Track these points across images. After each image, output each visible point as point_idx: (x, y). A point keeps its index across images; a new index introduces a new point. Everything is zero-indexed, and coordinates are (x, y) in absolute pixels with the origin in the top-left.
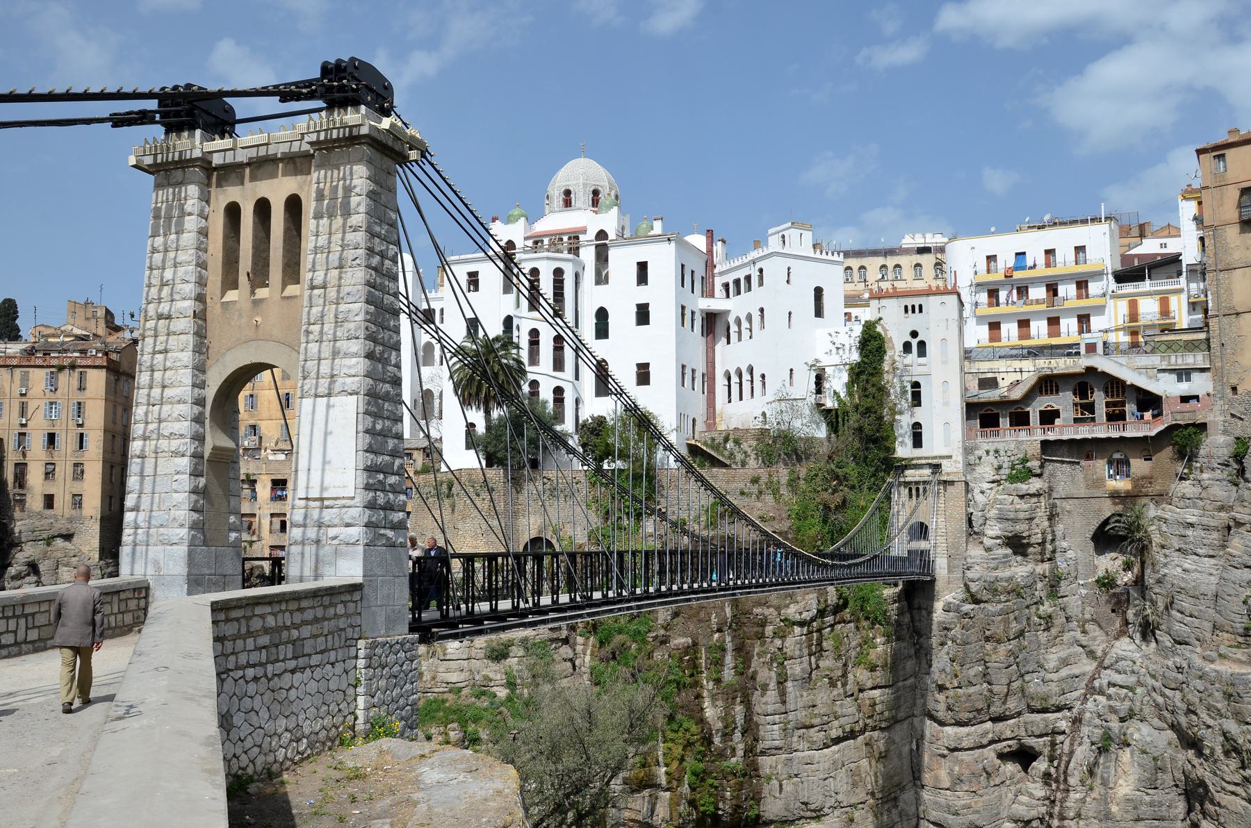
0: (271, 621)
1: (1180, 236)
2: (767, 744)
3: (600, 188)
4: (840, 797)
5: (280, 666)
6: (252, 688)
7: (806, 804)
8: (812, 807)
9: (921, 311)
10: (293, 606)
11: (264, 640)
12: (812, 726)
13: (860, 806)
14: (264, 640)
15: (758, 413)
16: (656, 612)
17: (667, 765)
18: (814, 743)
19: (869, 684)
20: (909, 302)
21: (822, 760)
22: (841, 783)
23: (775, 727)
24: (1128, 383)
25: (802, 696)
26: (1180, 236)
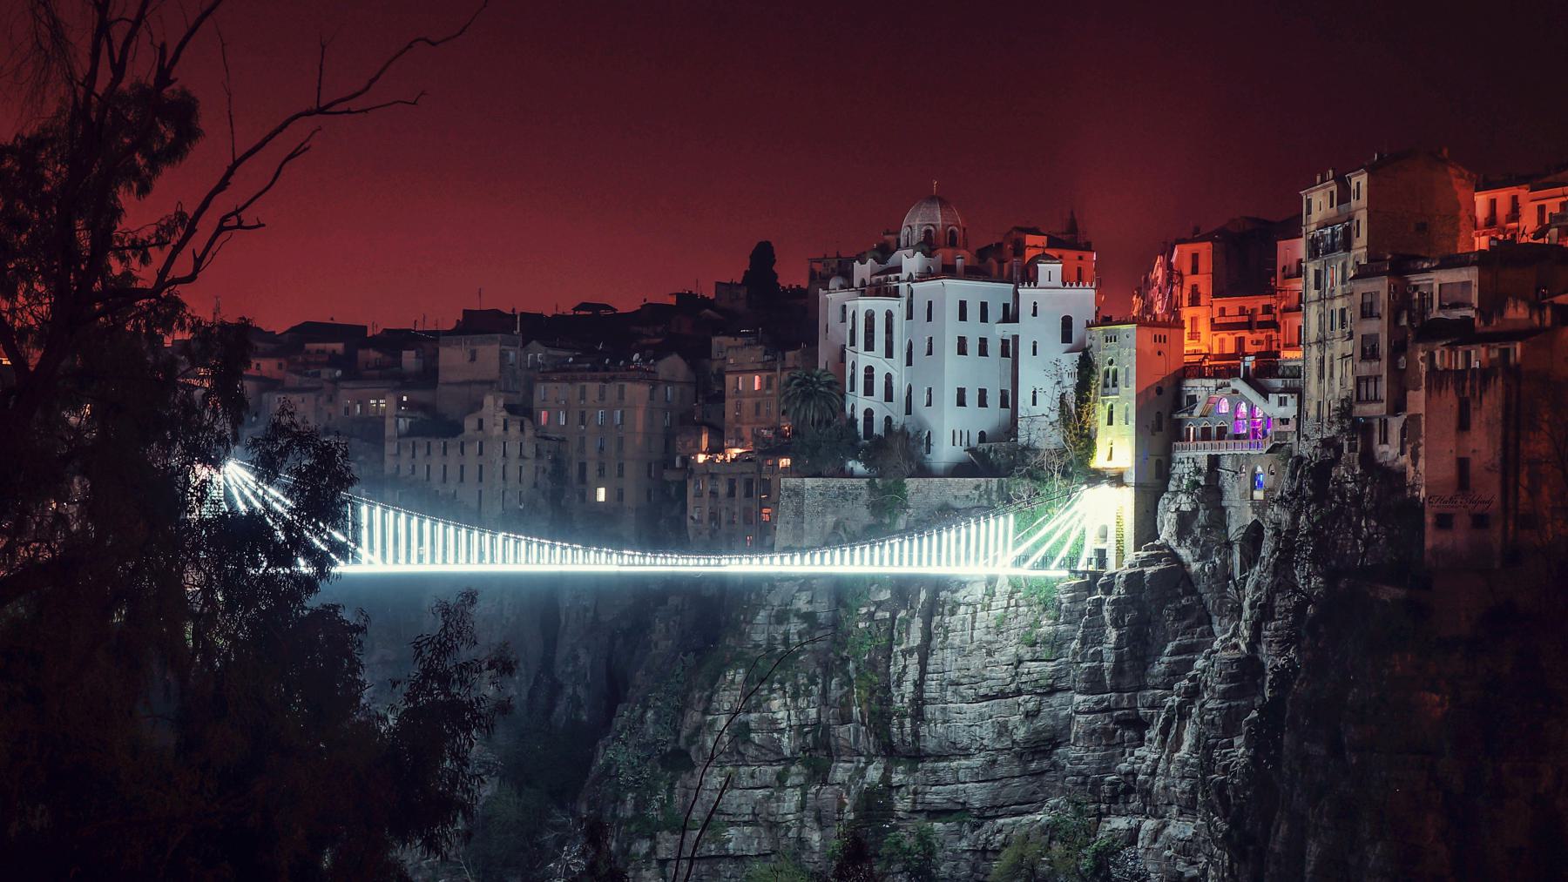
2: (757, 622)
4: (985, 742)
7: (954, 743)
8: (959, 746)
12: (962, 684)
13: (1006, 751)
15: (309, 421)
17: (859, 706)
18: (963, 697)
19: (1028, 657)
21: (968, 711)
22: (986, 733)
23: (934, 683)
25: (956, 660)
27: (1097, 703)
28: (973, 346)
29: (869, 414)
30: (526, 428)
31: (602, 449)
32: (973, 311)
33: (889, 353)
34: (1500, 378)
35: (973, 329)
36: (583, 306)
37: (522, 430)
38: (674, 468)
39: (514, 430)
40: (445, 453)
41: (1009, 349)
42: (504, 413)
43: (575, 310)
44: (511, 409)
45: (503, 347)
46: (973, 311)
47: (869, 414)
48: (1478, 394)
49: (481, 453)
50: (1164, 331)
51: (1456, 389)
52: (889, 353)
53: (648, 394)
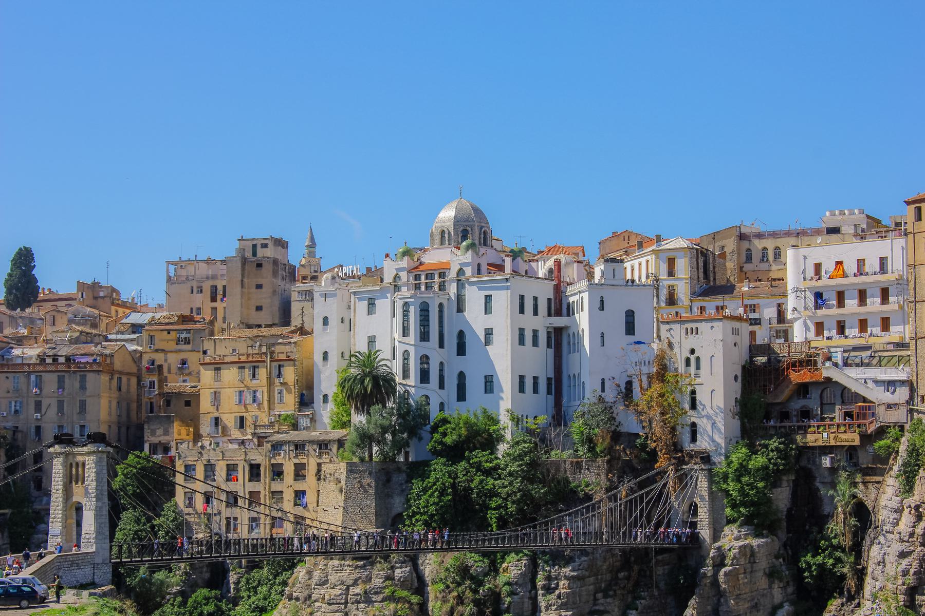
0: (71, 559)
1: (486, 392)
3: (468, 228)
5: (73, 568)
6: (67, 572)
9: (697, 333)
10: (76, 556)
11: (70, 563)
14: (70, 563)
16: (139, 567)
20: (689, 326)
24: (853, 391)
26: (486, 392)
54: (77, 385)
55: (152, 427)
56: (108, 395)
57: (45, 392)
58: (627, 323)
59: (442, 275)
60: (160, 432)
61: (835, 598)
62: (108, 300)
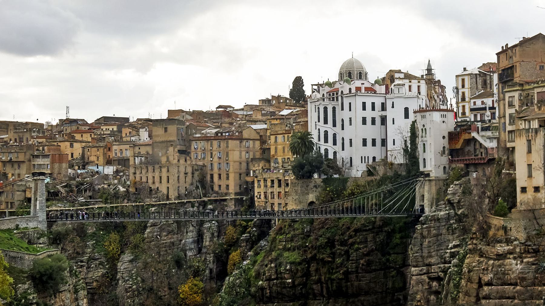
27: (421, 271)
28: (369, 121)
29: (326, 151)
30: (187, 160)
31: (220, 168)
32: (369, 106)
33: (334, 125)
34: (542, 132)
35: (369, 114)
36: (220, 107)
37: (186, 161)
38: (250, 176)
39: (182, 161)
40: (154, 171)
41: (384, 120)
42: (178, 154)
43: (217, 108)
44: (181, 152)
45: (178, 126)
46: (369, 106)
47: (326, 151)
48: (534, 138)
49: (168, 171)
50: (445, 113)
51: (526, 137)
52: (334, 125)
53: (239, 144)
54: (225, 145)
55: (254, 163)
56: (239, 149)
57: (213, 149)
58: (335, 117)
59: (337, 94)
60: (256, 165)
61: (119, 190)
62: (284, 104)
